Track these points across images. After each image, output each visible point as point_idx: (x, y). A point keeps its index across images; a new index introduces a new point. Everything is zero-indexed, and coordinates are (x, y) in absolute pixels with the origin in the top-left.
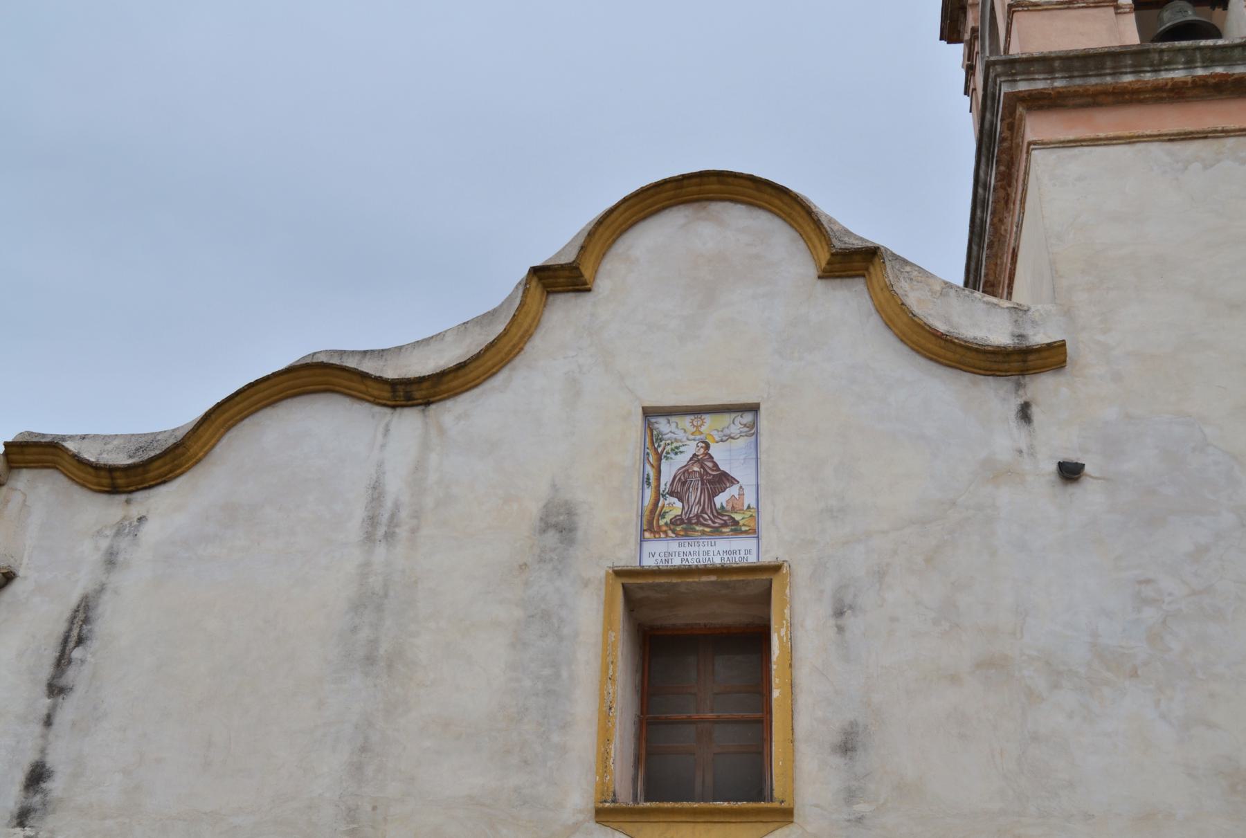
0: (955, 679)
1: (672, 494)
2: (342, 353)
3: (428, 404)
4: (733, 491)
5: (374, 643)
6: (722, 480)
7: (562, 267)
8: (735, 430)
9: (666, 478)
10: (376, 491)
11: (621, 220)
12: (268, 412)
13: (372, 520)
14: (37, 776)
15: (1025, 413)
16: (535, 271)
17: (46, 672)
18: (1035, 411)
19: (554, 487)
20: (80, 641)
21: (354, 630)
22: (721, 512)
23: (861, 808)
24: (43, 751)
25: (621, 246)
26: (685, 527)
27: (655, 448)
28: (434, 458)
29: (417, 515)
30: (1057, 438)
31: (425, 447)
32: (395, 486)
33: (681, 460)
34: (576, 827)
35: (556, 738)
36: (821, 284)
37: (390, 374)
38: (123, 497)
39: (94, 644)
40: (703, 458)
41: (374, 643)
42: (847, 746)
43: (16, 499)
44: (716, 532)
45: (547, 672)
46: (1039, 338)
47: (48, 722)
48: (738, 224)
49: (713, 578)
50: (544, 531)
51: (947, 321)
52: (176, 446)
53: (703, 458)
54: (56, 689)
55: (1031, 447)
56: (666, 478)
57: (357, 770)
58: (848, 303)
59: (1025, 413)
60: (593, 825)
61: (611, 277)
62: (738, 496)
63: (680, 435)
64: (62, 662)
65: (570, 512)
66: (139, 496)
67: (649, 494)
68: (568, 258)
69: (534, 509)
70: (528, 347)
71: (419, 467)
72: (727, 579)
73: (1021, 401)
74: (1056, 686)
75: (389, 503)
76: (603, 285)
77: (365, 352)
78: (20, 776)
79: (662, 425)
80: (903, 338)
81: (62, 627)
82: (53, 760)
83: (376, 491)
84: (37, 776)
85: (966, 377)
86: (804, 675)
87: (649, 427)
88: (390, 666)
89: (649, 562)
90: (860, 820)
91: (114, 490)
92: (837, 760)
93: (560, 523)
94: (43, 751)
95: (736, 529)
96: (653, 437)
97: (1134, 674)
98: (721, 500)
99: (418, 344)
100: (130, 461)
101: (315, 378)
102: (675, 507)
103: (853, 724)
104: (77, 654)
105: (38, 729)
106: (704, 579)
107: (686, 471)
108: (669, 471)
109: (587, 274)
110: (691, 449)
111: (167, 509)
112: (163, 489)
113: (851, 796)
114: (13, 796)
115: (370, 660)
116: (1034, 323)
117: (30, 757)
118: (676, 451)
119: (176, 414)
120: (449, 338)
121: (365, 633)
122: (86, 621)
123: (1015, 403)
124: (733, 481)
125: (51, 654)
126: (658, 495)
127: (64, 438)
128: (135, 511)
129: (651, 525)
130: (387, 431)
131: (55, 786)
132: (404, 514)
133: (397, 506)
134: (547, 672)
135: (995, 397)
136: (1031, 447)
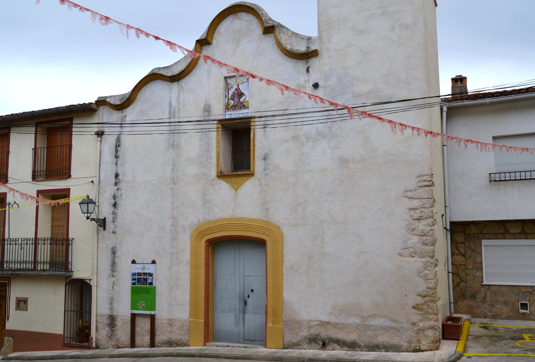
0: (287, 141)
1: (231, 99)
2: (159, 68)
3: (179, 80)
4: (244, 97)
5: (173, 142)
6: (241, 94)
7: (203, 39)
8: (245, 80)
9: (230, 95)
10: (170, 104)
11: (65, 156)
12: (146, 86)
13: (170, 112)
14: (117, 175)
15: (308, 70)
16: (198, 41)
17: (114, 153)
18: (310, 69)
19: (206, 101)
20: (119, 146)
21: (169, 139)
22: (241, 103)
23: (267, 172)
24: (117, 170)
25: (218, 30)
26: (234, 107)
27: (227, 87)
28: (181, 95)
29: (179, 110)
30: (314, 77)
31: (179, 92)
32: (174, 103)
33: (233, 90)
34: (214, 180)
35: (209, 161)
36: (263, 36)
37: (169, 74)
38: (121, 111)
39: (122, 146)
40: (238, 89)
41: (173, 142)
42: (265, 159)
43: (101, 113)
44: (241, 108)
45: (207, 146)
46: (313, 48)
47: (116, 164)
48: (245, 18)
49: (239, 121)
50: (204, 112)
51: (291, 45)
52: (128, 98)
53: (238, 89)
54: (117, 157)
55: (308, 79)
56: (230, 95)
57: (173, 170)
58: (269, 41)
59: (308, 70)
60: (217, 179)
61: (218, 39)
62: (246, 98)
63: (233, 83)
64: (117, 151)
65: (210, 107)
66: (124, 110)
67: (227, 99)
68: (204, 37)
69: (202, 106)
70: (199, 62)
71: (178, 98)
72: (242, 121)
73: (307, 67)
74: (308, 141)
75: (173, 107)
76: (214, 42)
77: (164, 68)
78: (114, 176)
79: (229, 81)
80: (282, 51)
81: (115, 143)
82: (119, 172)
83: (170, 104)
84: (117, 175)
85: (296, 60)
86: (257, 143)
87: (226, 81)
88: (177, 147)
89: (227, 117)
90: (267, 174)
91: (119, 110)
92: (263, 162)
93: (207, 109)
94: (117, 170)
95: (245, 108)
96: (227, 84)
97: (324, 137)
98: (241, 100)
99: (176, 63)
100: (120, 103)
101: (154, 77)
102: (232, 102)
103: (266, 153)
104: (119, 149)
105: (115, 166)
106: (237, 121)
107: (234, 93)
108: (231, 93)
109: (209, 40)
110: (235, 87)
111: (189, 82)
112: (128, 108)
113: (265, 169)
114: (113, 180)
115: (173, 146)
116: (312, 43)
117: (115, 172)
118: (232, 88)
119: (127, 88)
120: (182, 61)
121: (172, 140)
122: (119, 141)
123: (306, 67)
124: (244, 94)
125: (114, 149)
126: (228, 100)
127: (106, 97)
128: (124, 114)
129: (227, 108)
130: (171, 88)
131: (120, 177)
132: (176, 110)
133: (175, 108)
134: (207, 146)
135: (301, 65)
136: (308, 79)
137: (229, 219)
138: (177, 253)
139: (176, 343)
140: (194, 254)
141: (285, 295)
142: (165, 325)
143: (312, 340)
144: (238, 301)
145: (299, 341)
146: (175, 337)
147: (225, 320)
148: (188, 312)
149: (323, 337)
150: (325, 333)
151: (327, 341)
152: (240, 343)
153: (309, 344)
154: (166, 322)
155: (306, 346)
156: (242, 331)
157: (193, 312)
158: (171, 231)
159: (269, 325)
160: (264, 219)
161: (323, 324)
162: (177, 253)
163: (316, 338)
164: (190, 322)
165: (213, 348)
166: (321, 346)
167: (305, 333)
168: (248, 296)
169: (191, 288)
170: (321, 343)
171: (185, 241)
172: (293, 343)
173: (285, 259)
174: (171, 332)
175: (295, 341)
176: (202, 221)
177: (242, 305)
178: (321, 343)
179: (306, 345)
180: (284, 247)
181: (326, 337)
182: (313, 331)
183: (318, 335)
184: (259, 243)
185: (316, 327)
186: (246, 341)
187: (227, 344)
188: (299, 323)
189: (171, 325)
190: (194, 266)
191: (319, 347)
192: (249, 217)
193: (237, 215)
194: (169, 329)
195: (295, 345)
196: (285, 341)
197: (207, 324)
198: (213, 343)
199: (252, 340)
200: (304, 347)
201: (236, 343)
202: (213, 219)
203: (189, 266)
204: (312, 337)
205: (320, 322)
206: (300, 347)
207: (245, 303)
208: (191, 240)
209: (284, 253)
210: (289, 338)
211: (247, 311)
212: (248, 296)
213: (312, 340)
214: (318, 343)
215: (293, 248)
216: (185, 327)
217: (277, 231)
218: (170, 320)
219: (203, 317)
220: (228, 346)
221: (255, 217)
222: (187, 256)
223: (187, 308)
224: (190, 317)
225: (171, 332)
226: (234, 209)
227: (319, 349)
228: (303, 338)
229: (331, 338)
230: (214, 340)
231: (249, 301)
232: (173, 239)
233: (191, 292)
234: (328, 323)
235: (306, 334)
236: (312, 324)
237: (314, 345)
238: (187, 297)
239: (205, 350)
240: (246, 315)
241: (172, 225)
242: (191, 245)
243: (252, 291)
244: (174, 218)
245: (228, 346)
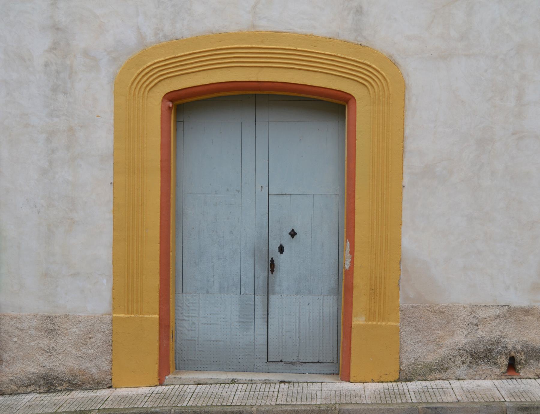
137: (238, 35)
138: (71, 129)
139: (69, 382)
140: (126, 130)
141: (408, 241)
142: (33, 332)
143: (480, 356)
144: (251, 261)
145: (443, 359)
146: (63, 365)
147: (212, 314)
148: (107, 294)
149: (510, 347)
150: (514, 338)
151: (521, 357)
152: (254, 370)
153: (470, 367)
154: (33, 323)
155: (462, 371)
156: (261, 339)
157: (125, 293)
158: (46, 65)
159: (358, 321)
160: (351, 37)
161: (514, 314)
162: (71, 129)
163: (490, 350)
164: (113, 321)
165: (190, 387)
166: (504, 368)
167: (462, 338)
168: (281, 249)
169: (115, 228)
170: (506, 362)
171: (97, 98)
172: (426, 365)
173: (410, 145)
174: (50, 353)
175: (431, 359)
176: (150, 38)
177: (262, 272)
178: (504, 361)
179: (464, 367)
180: (408, 114)
181: (518, 347)
182: (485, 333)
183: (498, 342)
184: (334, 106)
185: (493, 323)
186: (272, 366)
187: (230, 376)
188: (446, 315)
189: (50, 331)
190: (126, 167)
191: (498, 372)
192: (304, 31)
193: (264, 25)
194: (44, 343)
195: (431, 370)
196: (405, 362)
197: (165, 325)
198: (186, 376)
199: (291, 363)
200: (458, 373)
201: (245, 371)
202: (187, 34)
203: (109, 166)
204: (480, 348)
205: (505, 310)
206: (444, 375)
207: (272, 266)
208: (116, 94)
209: (407, 131)
210: (416, 351)
211: (277, 288)
212: (281, 249)
213: (480, 356)
214: (495, 363)
215: (434, 120)
216: (99, 336)
217: (385, 75)
218: (50, 318)
219: (156, 306)
220: (233, 382)
221: (321, 31)
222: (102, 138)
223: (105, 286)
224: (114, 309)
225: (50, 353)
226: (254, 7)
227: (499, 378)
228: (454, 353)
229: (533, 348)
230: (179, 368)
231: (281, 261)
232: (55, 90)
233: (115, 240)
234: (527, 311)
235: (464, 341)
236: (482, 314)
237: (485, 367)
238: (103, 252)
239: (163, 397)
240: (272, 298)
241: (54, 48)
242: (117, 107)
243: (293, 234)
244: (56, 28)
245: (233, 382)
